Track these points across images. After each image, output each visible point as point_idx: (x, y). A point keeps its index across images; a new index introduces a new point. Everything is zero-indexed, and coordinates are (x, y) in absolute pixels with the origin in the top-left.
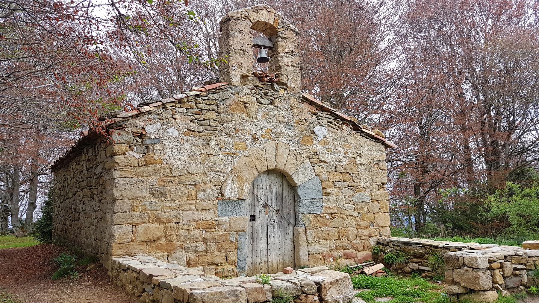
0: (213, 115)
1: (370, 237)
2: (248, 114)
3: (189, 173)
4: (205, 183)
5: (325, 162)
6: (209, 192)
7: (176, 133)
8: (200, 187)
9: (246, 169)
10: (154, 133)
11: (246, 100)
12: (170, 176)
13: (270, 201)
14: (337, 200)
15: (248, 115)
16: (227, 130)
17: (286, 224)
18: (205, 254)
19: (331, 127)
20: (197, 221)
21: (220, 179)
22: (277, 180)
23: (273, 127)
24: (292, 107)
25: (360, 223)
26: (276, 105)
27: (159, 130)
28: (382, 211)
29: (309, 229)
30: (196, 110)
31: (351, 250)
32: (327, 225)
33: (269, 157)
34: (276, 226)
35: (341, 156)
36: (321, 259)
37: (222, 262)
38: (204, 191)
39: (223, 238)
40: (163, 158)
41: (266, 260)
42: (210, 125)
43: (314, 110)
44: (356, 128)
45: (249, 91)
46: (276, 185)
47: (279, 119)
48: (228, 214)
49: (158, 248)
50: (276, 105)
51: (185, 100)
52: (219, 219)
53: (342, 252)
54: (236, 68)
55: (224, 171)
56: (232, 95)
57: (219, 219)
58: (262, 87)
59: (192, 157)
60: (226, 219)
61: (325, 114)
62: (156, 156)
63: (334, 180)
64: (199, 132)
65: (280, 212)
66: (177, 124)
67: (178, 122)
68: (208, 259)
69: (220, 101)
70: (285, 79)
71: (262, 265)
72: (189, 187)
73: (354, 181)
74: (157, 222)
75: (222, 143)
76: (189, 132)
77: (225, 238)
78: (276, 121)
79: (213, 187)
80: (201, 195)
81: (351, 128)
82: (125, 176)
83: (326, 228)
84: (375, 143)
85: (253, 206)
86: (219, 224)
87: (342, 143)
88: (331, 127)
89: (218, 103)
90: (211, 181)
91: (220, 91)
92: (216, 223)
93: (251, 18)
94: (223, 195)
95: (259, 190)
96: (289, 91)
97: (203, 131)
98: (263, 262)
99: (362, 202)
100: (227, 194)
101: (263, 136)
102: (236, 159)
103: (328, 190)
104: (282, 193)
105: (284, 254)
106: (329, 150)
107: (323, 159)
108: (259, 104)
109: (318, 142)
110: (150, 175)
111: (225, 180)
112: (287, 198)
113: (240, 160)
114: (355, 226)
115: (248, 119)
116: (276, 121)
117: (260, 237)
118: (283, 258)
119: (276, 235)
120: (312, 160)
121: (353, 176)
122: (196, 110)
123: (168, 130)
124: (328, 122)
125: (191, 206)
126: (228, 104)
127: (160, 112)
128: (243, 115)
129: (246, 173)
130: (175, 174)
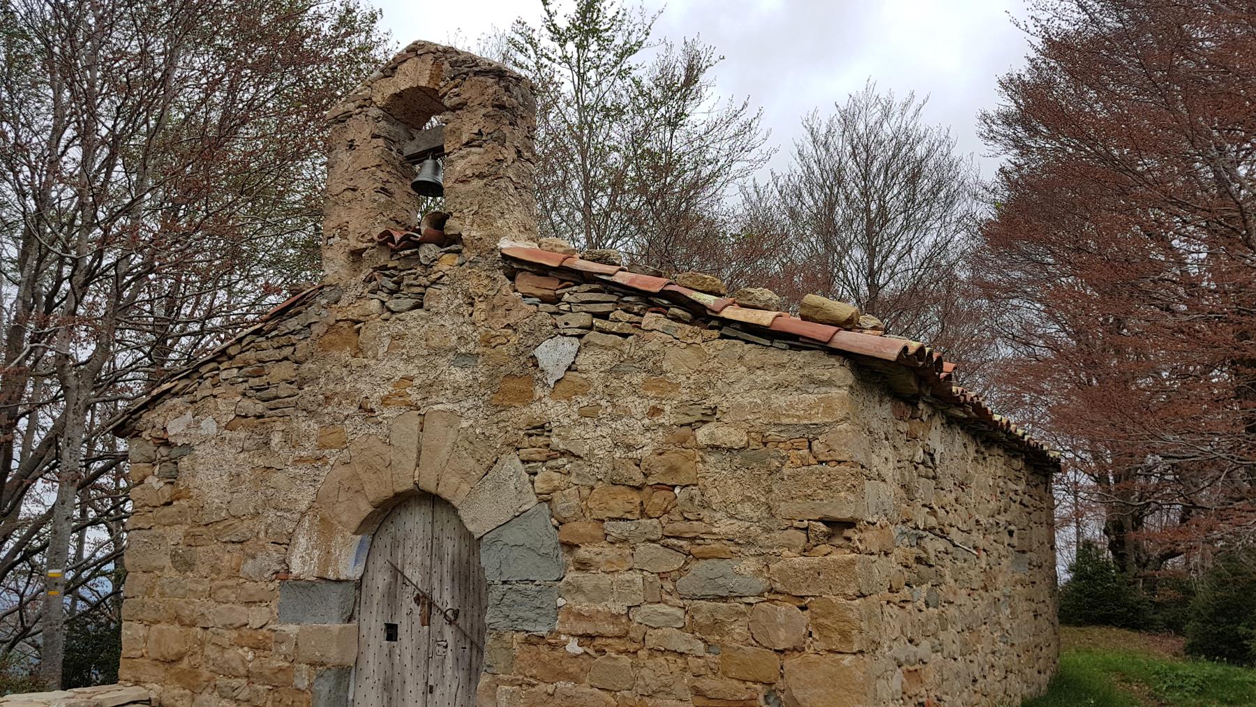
11: (354, 313)
13: (436, 585)
14: (615, 584)
19: (602, 331)
28: (820, 645)
29: (504, 682)
34: (449, 662)
35: (634, 427)
43: (549, 286)
44: (700, 316)
47: (431, 343)
50: (426, 305)
56: (324, 312)
58: (395, 268)
60: (292, 629)
61: (583, 292)
65: (460, 621)
69: (299, 332)
81: (676, 319)
82: (140, 525)
83: (564, 686)
84: (785, 357)
85: (391, 597)
95: (408, 551)
101: (385, 401)
103: (582, 553)
104: (468, 562)
106: (589, 413)
108: (386, 315)
115: (354, 362)
116: (425, 353)
124: (595, 315)
128: (346, 355)
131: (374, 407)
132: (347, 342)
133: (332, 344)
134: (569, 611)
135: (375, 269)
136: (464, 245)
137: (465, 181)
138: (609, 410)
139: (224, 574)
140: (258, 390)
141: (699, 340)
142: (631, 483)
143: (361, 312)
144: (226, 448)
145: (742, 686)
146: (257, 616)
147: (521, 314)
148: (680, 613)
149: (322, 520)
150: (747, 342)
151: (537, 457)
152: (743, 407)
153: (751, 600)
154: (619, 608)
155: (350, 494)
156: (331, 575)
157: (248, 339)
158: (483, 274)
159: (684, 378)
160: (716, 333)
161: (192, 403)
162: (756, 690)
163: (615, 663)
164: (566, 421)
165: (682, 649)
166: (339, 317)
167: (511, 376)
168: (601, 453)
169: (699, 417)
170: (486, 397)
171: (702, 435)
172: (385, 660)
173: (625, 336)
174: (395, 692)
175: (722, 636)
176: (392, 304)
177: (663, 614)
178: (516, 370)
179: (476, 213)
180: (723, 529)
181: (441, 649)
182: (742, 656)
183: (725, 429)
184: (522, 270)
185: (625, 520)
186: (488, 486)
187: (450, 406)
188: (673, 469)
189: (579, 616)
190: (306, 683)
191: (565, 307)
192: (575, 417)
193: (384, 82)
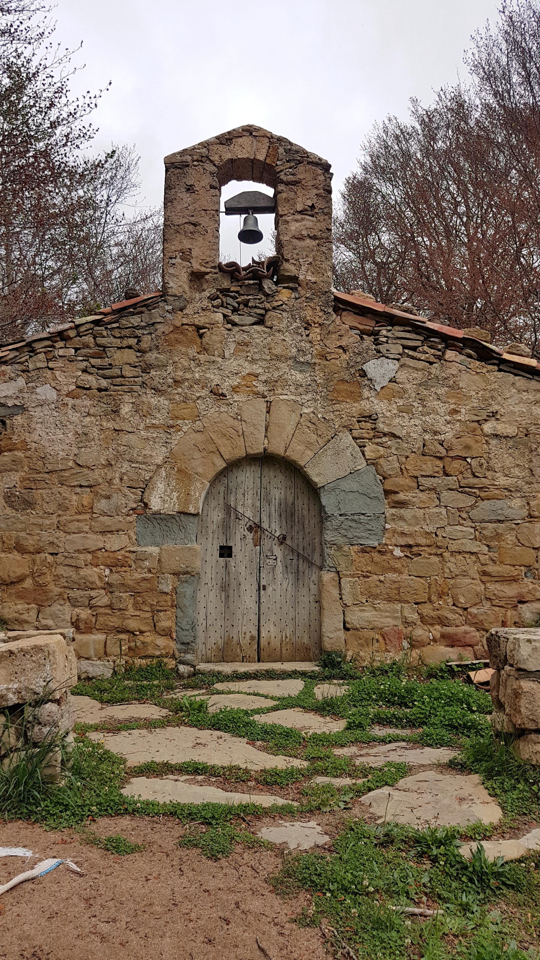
0: (130, 356)
1: (521, 602)
2: (205, 349)
3: (79, 465)
4: (110, 482)
5: (394, 436)
6: (117, 499)
7: (52, 395)
8: (100, 491)
9: (197, 455)
10: (11, 397)
11: (200, 320)
12: (42, 471)
13: (265, 518)
14: (422, 516)
15: (205, 349)
16: (155, 382)
17: (303, 566)
18: (109, 612)
19: (413, 358)
20: (94, 552)
21: (140, 474)
22: (281, 477)
23: (260, 371)
24: (308, 326)
25: (490, 569)
26: (269, 323)
27: (21, 391)
29: (346, 576)
30: (96, 350)
31: (466, 628)
32: (395, 570)
33: (248, 430)
35: (439, 421)
36: (378, 641)
37: (143, 628)
38: (108, 497)
39: (144, 585)
40: (28, 440)
41: (255, 633)
42: (123, 377)
43: (369, 324)
44: (485, 355)
45: (206, 303)
46: (279, 488)
47: (274, 351)
48: (158, 539)
49: (20, 596)
50: (269, 323)
51: (72, 333)
52: (139, 549)
53: (437, 630)
54: (178, 260)
55: (148, 460)
56: (169, 315)
57: (139, 549)
58: (237, 292)
59: (83, 437)
60: (154, 550)
61: (398, 331)
62: (15, 437)
63: (416, 473)
64: (100, 390)
65: (288, 542)
66: (55, 379)
67: (57, 373)
68: (114, 621)
69: (143, 328)
70: (293, 268)
71: (245, 642)
72: (78, 490)
73: (475, 476)
74: (18, 552)
75: (145, 408)
76: (79, 390)
77: (149, 586)
78: (268, 358)
79: (126, 490)
80: (103, 505)
81: (469, 356)
85: (226, 527)
86: (140, 559)
87: (441, 391)
88: (413, 358)
89: (139, 332)
90: (121, 479)
91: (144, 309)
92: (132, 556)
93: (215, 158)
94: (146, 505)
95: (240, 496)
96: (303, 292)
97: (109, 389)
98: (248, 636)
99: (500, 521)
100: (155, 504)
101: (235, 389)
102: (176, 438)
103: (401, 496)
104: (293, 503)
105: (296, 626)
106: (406, 410)
107: (386, 430)
108: (229, 326)
109: (373, 393)
110: (6, 470)
111: (151, 478)
112: (305, 513)
113: (185, 437)
114: (477, 576)
115: (203, 358)
116: (268, 358)
117: (243, 588)
118: (294, 632)
119: (280, 585)
120: (356, 433)
121: (474, 463)
122: (96, 350)
123: (38, 390)
125: (81, 524)
126: (159, 332)
127: (23, 359)
128: (192, 352)
129: (198, 462)
130: (50, 468)
131: (225, 391)
132: (192, 342)
133: (178, 341)
134: (394, 531)
135: (218, 290)
136: (300, 285)
137: (301, 238)
138: (420, 409)
139: (73, 511)
140: (99, 369)
141: (484, 370)
142: (438, 455)
143: (207, 321)
144: (70, 412)
145: (513, 568)
146: (114, 543)
147: (351, 340)
148: (472, 530)
149: (179, 471)
150: (516, 375)
151: (366, 435)
152: (515, 413)
153: (519, 521)
154: (431, 529)
155: (204, 453)
156: (192, 510)
157: (88, 326)
158: (318, 308)
159: (474, 393)
160: (496, 368)
161: (23, 371)
162: (521, 570)
163: (428, 561)
164: (388, 414)
165: (475, 550)
166: (185, 321)
167: (343, 381)
168: (415, 436)
169: (485, 417)
170: (323, 394)
171: (488, 427)
172: (223, 571)
173: (431, 363)
174: (231, 592)
175: (499, 542)
176: (236, 318)
177: (462, 531)
178: (347, 378)
179: (310, 264)
180: (502, 482)
181: (271, 562)
182: (514, 552)
183: (503, 425)
184: (344, 310)
185: (434, 477)
186: (330, 452)
187: (293, 397)
188: (467, 447)
189: (403, 534)
190: (171, 587)
191: (384, 339)
192: (395, 412)
193: (221, 147)
